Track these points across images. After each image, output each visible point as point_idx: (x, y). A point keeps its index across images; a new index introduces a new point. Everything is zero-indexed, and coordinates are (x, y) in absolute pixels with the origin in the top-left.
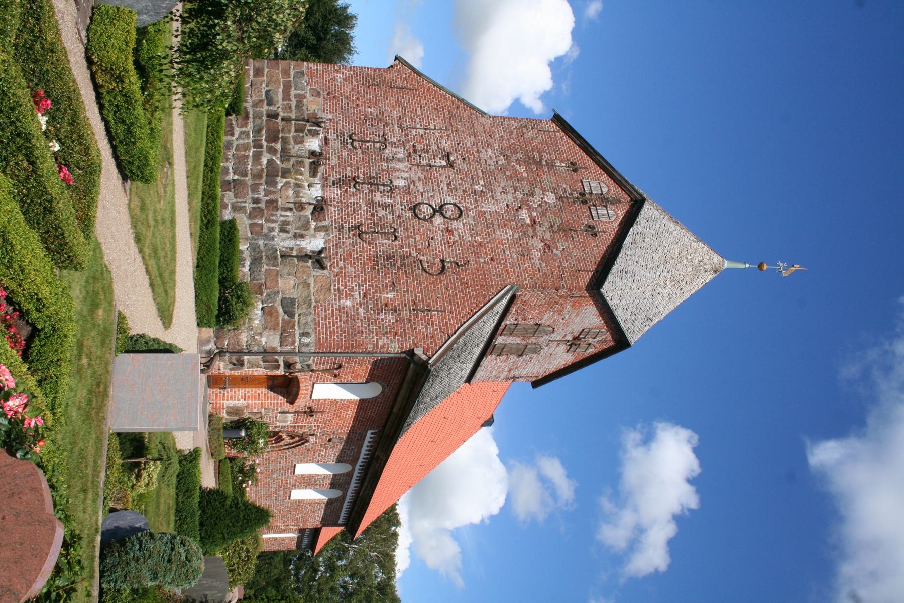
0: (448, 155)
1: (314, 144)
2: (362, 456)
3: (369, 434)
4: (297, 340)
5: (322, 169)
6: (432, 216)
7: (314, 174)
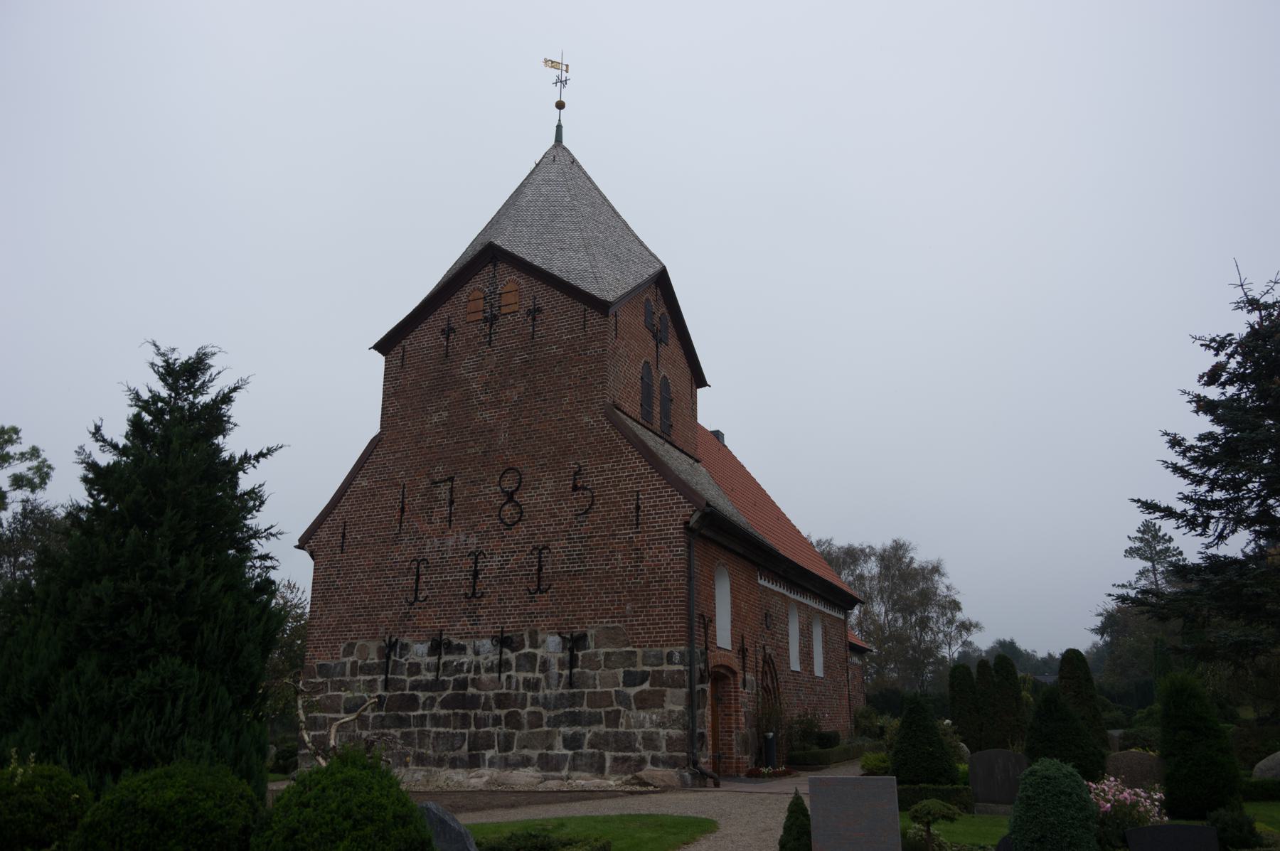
0: (435, 483)
1: (419, 651)
2: (781, 590)
3: (761, 582)
4: (676, 668)
5: (455, 641)
6: (518, 504)
7: (462, 649)
